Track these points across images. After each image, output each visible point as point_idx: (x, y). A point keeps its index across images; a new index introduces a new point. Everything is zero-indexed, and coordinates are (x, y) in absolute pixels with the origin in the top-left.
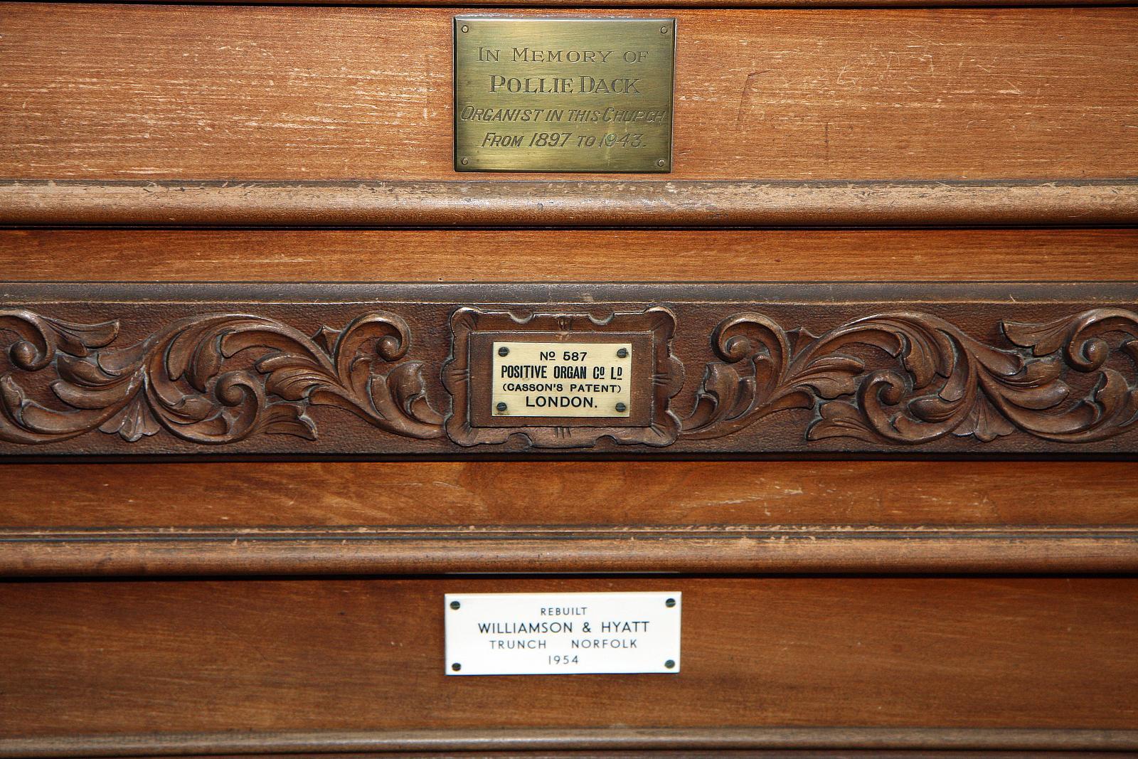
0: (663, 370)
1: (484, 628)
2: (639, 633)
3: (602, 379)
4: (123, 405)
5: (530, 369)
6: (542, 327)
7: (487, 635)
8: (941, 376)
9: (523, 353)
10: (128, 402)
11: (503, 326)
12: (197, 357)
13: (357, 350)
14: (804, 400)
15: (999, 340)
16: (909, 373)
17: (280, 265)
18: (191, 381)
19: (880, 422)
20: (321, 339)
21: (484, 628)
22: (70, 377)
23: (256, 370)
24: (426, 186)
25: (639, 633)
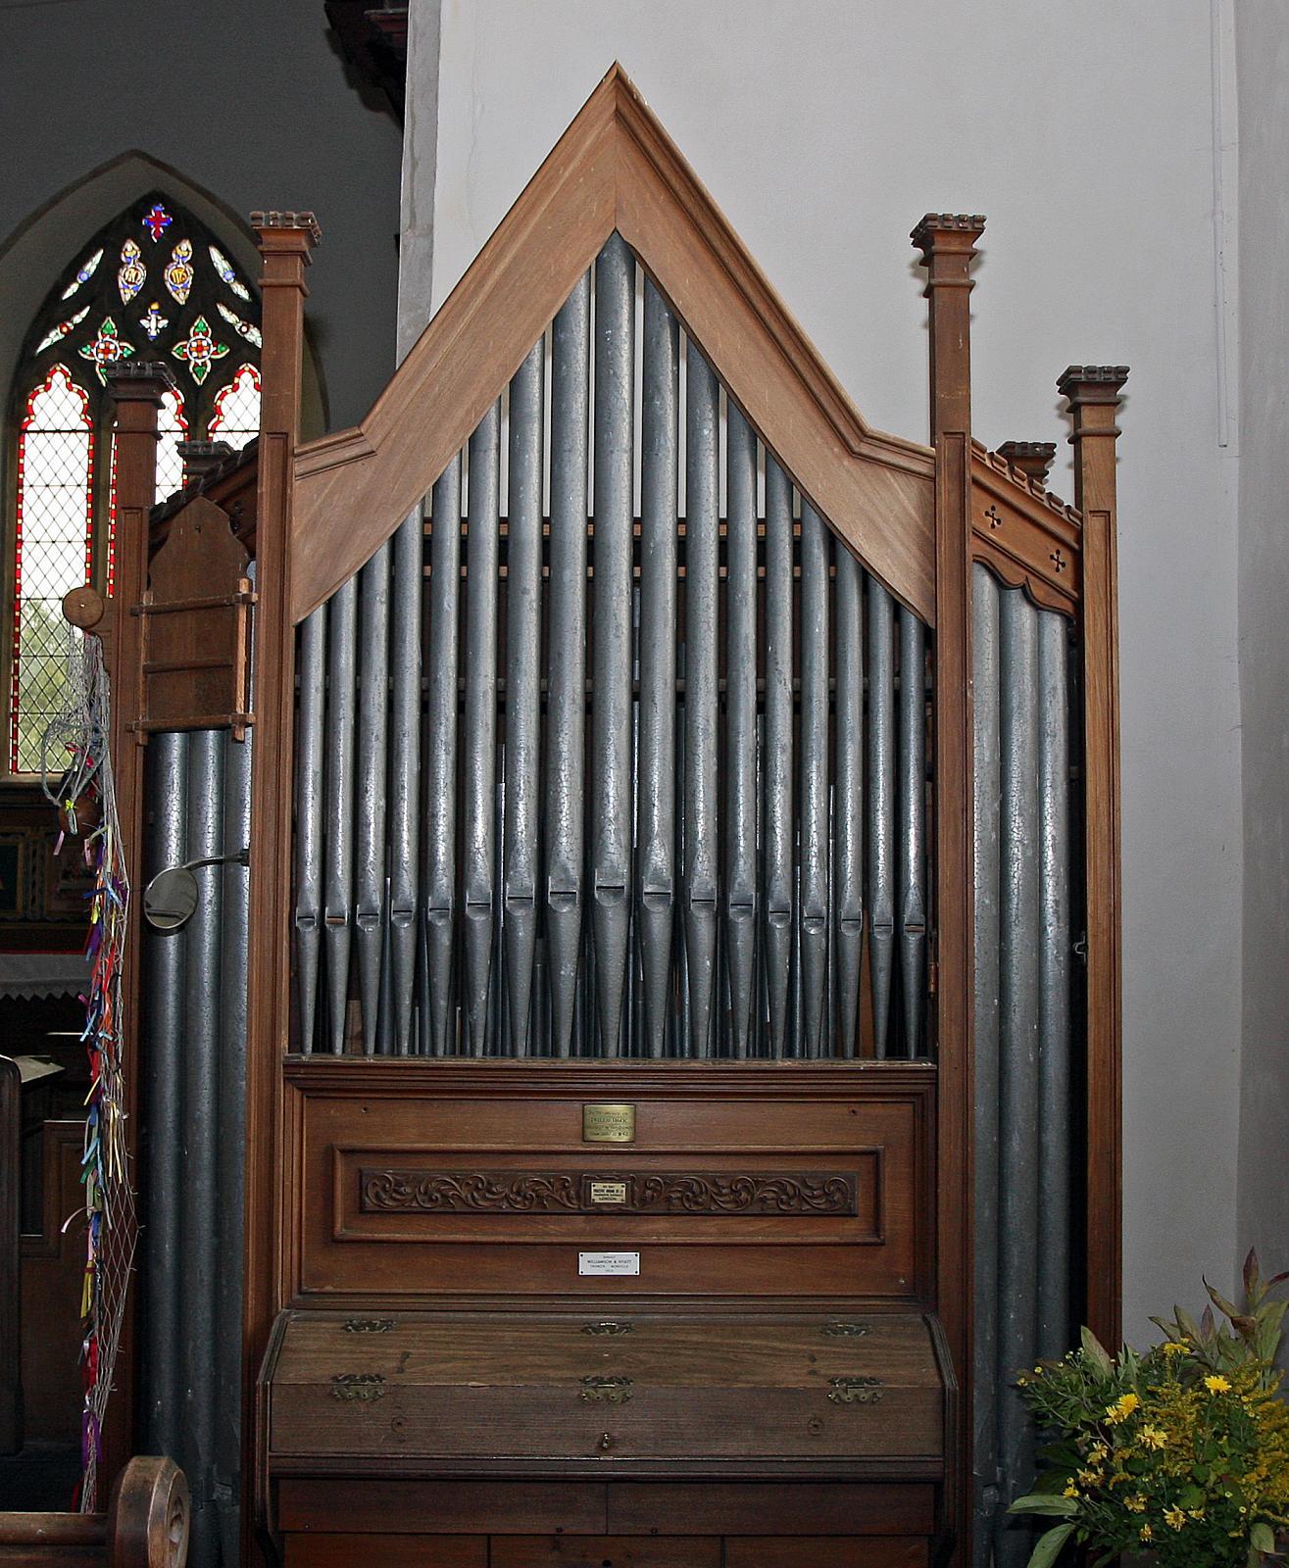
0: (633, 1191)
1: (945, 246)
2: (627, 1264)
3: (617, 1193)
4: (502, 1199)
5: (417, 1052)
6: (603, 1180)
7: (590, 1264)
8: (701, 1193)
9: (599, 1186)
10: (502, 1199)
11: (595, 1180)
12: (519, 1187)
13: (558, 1185)
14: (763, 1200)
15: (715, 1184)
16: (693, 1193)
17: (541, 1164)
18: (518, 1193)
19: (687, 1205)
20: (549, 1182)
21: (945, 246)
22: (396, 1191)
23: (533, 1191)
24: (577, 1145)
25: (627, 1264)
